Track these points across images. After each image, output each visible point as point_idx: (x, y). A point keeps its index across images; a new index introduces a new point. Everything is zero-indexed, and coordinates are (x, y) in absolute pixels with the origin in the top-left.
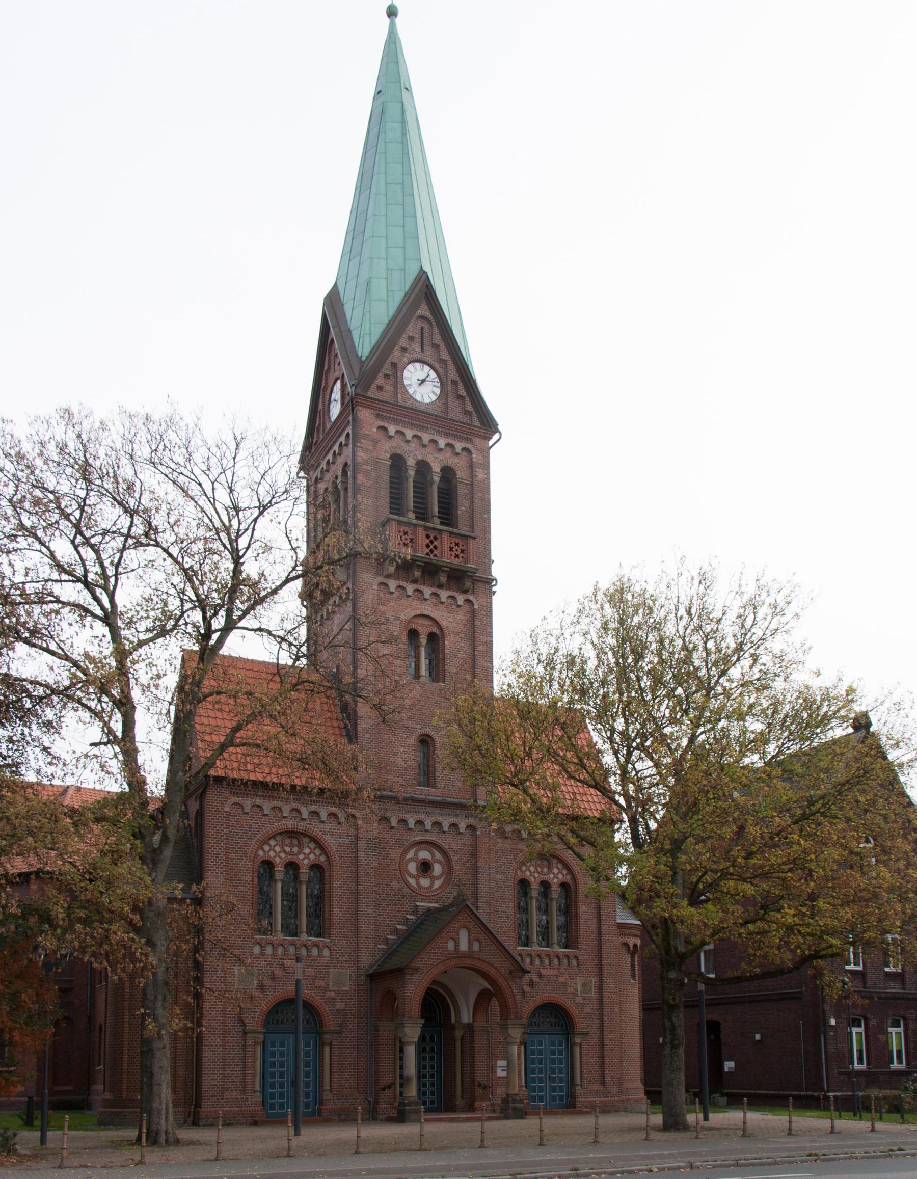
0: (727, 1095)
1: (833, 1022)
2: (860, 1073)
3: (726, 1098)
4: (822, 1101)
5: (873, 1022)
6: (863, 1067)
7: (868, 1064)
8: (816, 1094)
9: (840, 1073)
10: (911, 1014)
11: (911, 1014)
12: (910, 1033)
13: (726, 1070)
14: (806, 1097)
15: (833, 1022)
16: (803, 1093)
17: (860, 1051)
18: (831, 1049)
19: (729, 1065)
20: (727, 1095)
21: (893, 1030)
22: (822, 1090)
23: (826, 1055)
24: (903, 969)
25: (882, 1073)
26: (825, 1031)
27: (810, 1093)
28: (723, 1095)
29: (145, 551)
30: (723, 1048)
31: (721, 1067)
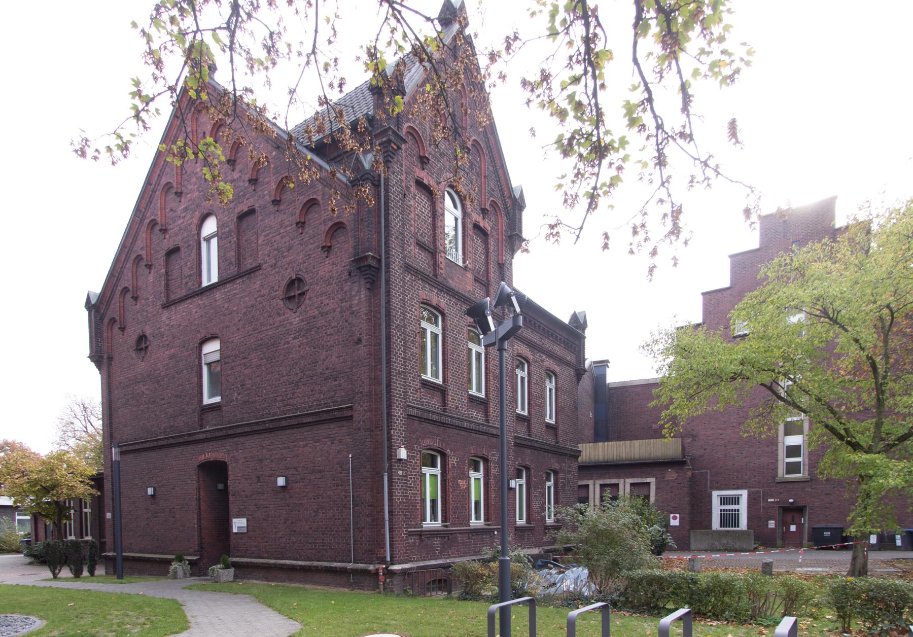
0: (235, 565)
1: (403, 453)
2: (433, 533)
3: (232, 570)
4: (381, 578)
5: (453, 461)
6: (438, 524)
7: (445, 519)
8: (371, 567)
9: (410, 534)
10: (493, 455)
11: (493, 455)
12: (492, 479)
13: (235, 530)
14: (355, 572)
15: (403, 453)
16: (350, 566)
17: (434, 502)
18: (398, 498)
19: (239, 524)
20: (235, 565)
21: (473, 475)
22: (383, 560)
23: (390, 506)
24: (556, 422)
25: (461, 532)
26: (390, 467)
27: (361, 566)
28: (227, 567)
29: (761, 633)
30: (231, 499)
31: (228, 525)
